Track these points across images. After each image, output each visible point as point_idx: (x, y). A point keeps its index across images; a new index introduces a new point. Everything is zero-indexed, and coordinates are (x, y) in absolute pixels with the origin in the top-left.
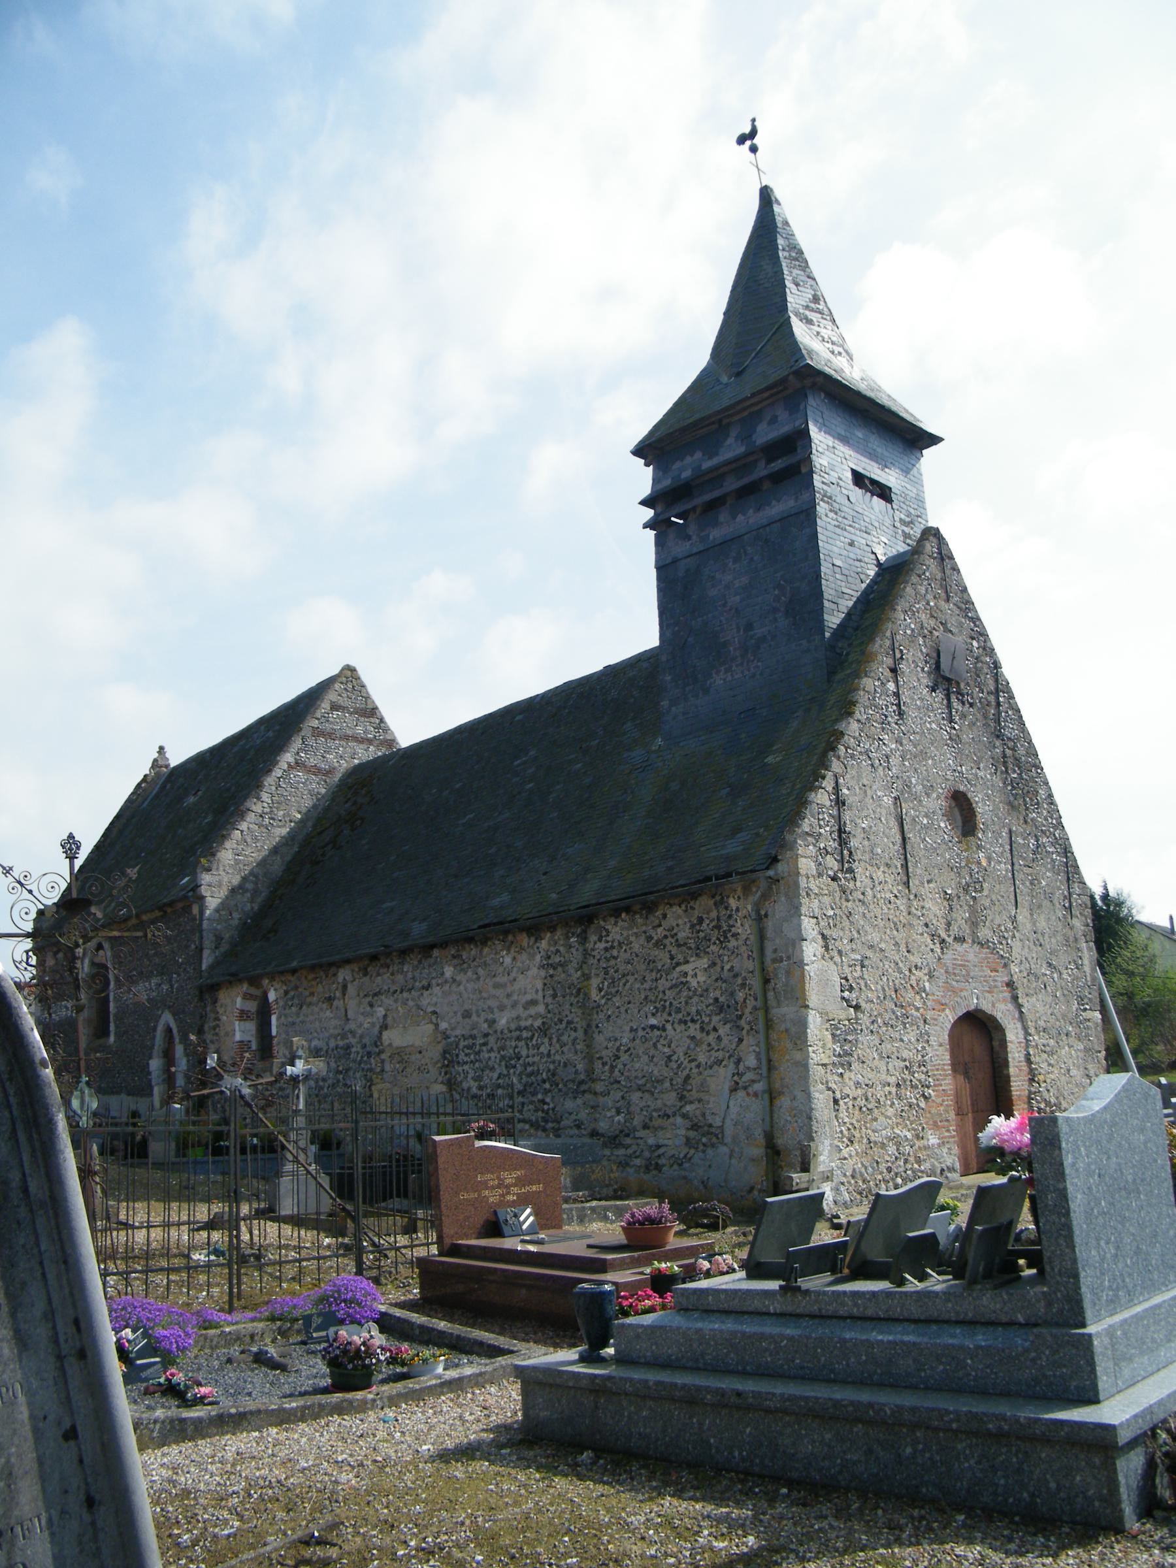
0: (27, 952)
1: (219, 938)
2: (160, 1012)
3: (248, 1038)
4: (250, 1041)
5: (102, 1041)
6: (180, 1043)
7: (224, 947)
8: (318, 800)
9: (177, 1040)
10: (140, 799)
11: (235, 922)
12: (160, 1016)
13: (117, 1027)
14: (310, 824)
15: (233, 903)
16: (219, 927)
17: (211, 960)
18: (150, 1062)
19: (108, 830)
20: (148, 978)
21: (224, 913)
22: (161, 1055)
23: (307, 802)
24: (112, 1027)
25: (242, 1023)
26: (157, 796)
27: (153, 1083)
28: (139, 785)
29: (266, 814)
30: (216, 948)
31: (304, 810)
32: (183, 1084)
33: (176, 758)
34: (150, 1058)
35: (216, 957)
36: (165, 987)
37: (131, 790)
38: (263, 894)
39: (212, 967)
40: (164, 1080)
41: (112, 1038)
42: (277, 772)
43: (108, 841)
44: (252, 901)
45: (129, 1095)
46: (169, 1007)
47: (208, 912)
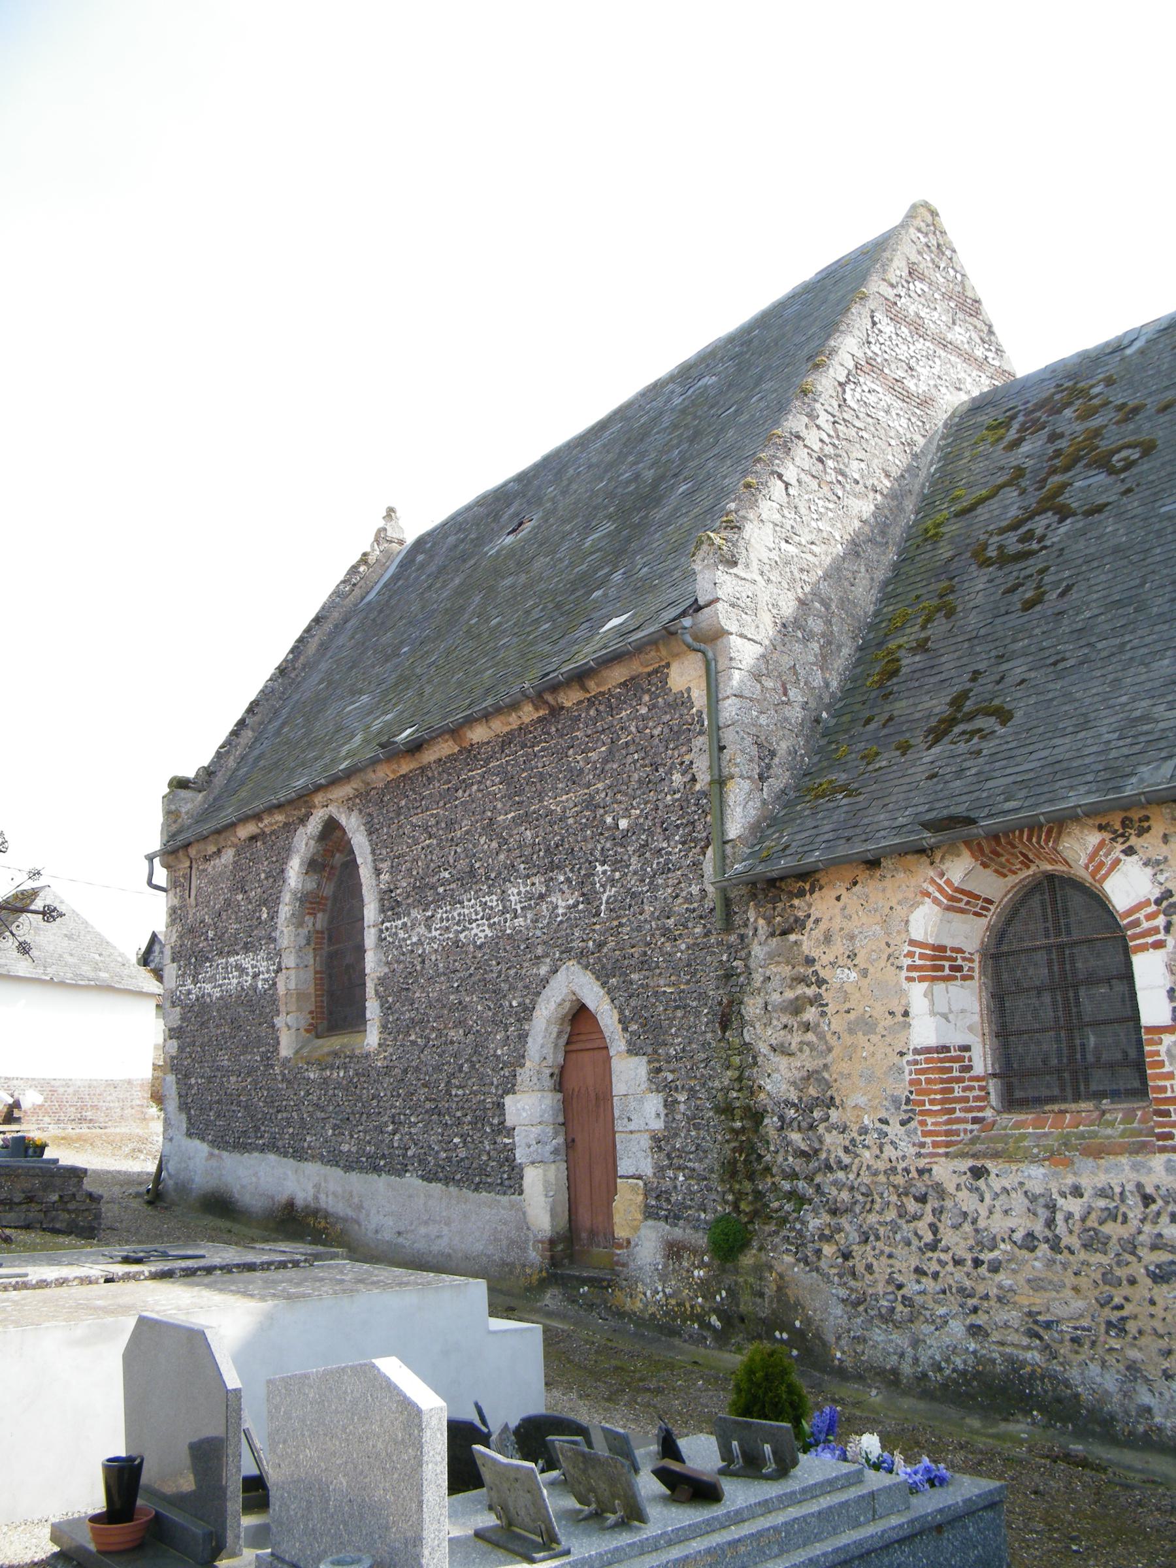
0: (150, 858)
1: (766, 753)
2: (543, 970)
3: (956, 1038)
4: (967, 1048)
5: (335, 1043)
6: (633, 1050)
7: (780, 779)
8: (915, 456)
9: (618, 1043)
10: (357, 591)
11: (796, 714)
12: (544, 982)
13: (386, 1009)
14: (910, 505)
15: (786, 661)
16: (763, 720)
17: (753, 811)
18: (508, 1100)
19: (301, 640)
20: (499, 879)
21: (769, 684)
22: (548, 1083)
23: (898, 461)
24: (373, 1008)
25: (940, 987)
26: (395, 578)
27: (520, 1156)
28: (354, 569)
29: (829, 457)
30: (762, 778)
31: (895, 472)
32: (647, 1168)
33: (412, 529)
34: (509, 1087)
35: (764, 802)
36: (562, 902)
37: (341, 576)
38: (845, 651)
39: (759, 830)
40: (555, 1152)
41: (372, 1038)
42: (837, 371)
43: (302, 659)
44: (824, 661)
45: (429, 1178)
46: (582, 955)
47: (737, 676)
